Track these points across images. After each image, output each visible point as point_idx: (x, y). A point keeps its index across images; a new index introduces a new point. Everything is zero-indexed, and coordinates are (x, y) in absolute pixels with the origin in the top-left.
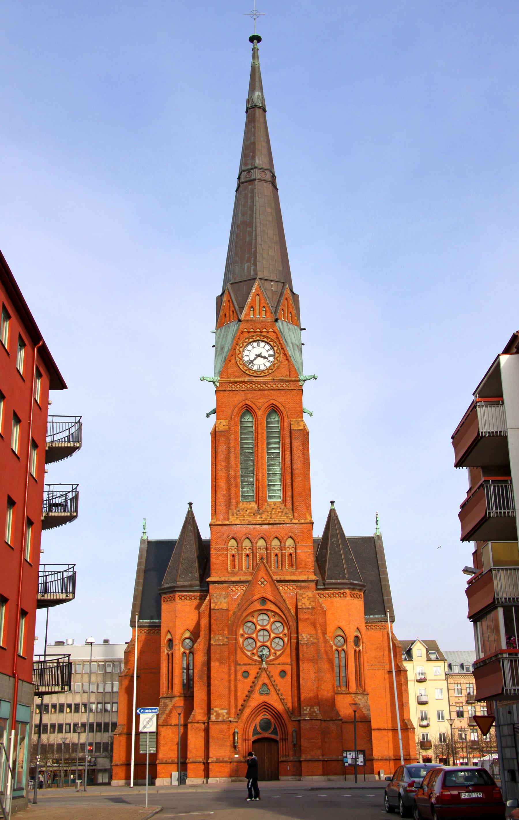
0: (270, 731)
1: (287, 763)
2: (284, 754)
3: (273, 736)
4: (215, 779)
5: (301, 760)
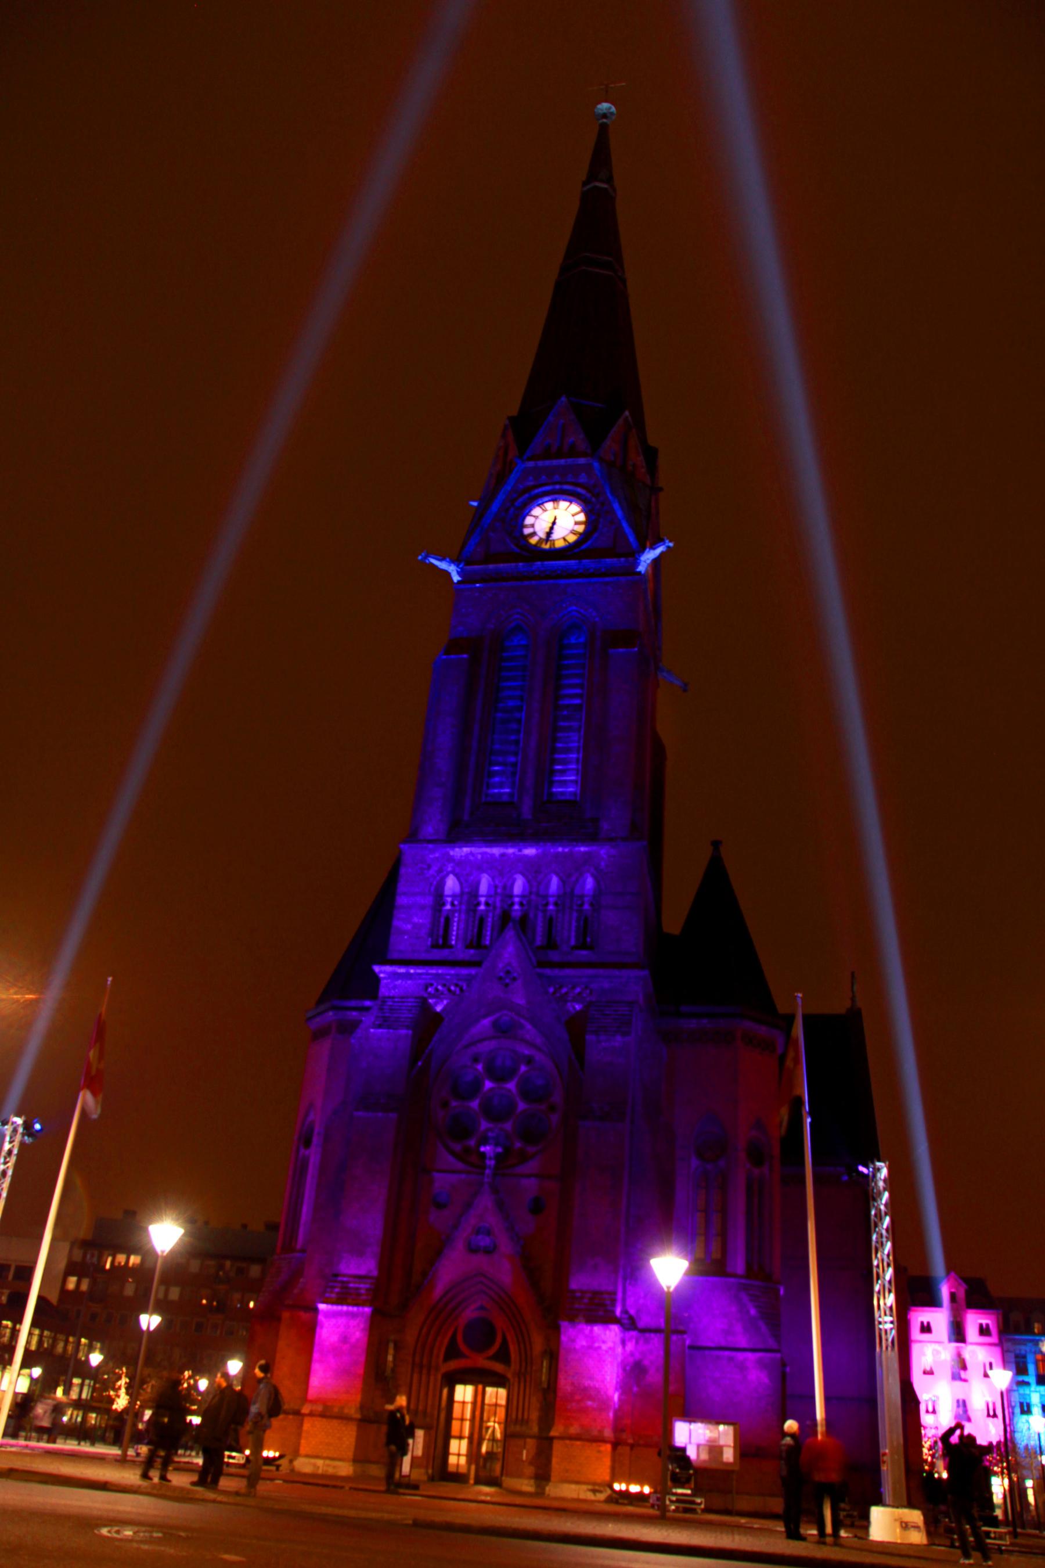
0: (493, 1351)
2: (520, 1416)
3: (498, 1367)
4: (313, 1461)
5: (553, 1433)
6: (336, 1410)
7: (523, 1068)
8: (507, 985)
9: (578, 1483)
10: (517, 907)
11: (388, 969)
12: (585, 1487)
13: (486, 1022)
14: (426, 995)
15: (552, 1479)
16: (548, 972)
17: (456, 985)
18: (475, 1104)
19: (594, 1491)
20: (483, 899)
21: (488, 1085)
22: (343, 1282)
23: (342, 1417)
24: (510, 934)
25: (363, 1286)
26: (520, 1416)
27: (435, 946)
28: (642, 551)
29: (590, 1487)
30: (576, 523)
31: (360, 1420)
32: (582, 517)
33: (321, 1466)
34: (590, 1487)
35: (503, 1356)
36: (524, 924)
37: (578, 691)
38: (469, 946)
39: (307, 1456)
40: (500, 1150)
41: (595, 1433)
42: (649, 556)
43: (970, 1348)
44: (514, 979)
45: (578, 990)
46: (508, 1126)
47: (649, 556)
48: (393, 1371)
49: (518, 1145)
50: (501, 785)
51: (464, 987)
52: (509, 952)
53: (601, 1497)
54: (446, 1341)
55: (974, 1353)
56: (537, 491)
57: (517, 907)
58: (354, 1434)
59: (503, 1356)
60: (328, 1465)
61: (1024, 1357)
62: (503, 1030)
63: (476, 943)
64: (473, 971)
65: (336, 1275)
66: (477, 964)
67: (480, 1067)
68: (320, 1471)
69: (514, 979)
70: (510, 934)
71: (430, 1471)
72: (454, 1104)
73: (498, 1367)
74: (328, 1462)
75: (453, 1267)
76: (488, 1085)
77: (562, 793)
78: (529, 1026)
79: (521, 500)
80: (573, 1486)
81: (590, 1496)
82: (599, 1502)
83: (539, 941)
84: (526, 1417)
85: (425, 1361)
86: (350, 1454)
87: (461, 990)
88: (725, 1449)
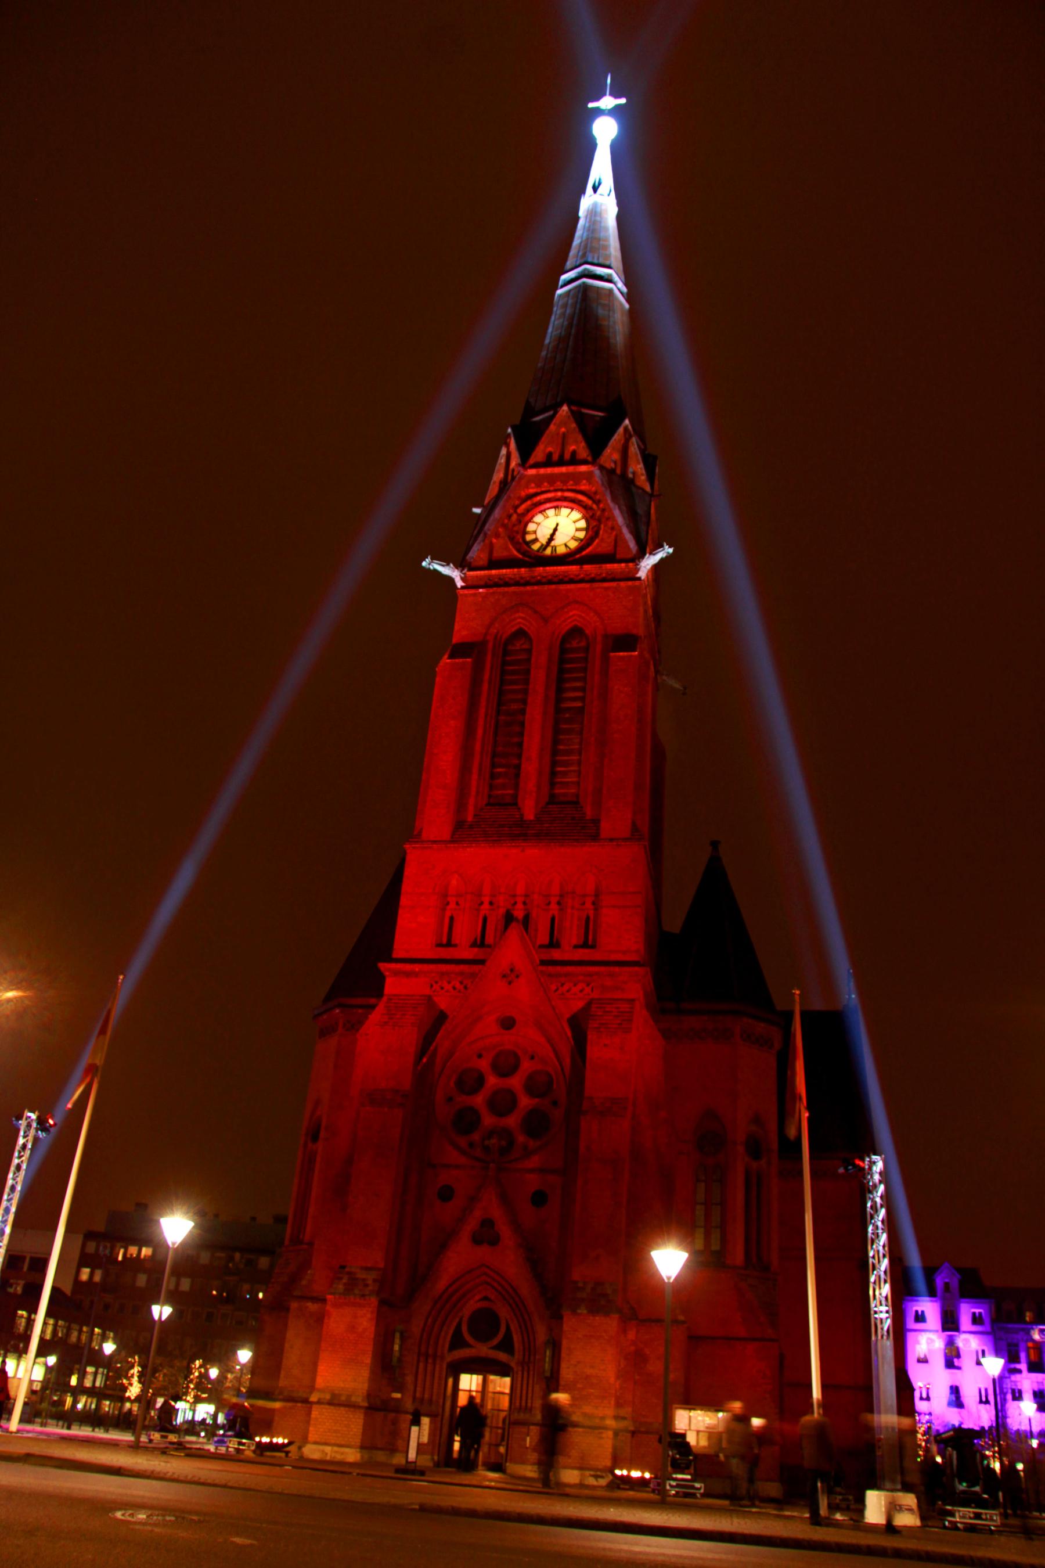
0: (495, 1341)
1: (524, 1430)
2: (523, 1404)
3: (502, 1356)
4: (321, 1447)
6: (343, 1398)
8: (510, 983)
19: (596, 1477)
25: (370, 1277)
26: (523, 1404)
28: (641, 555)
29: (592, 1473)
30: (577, 530)
31: (367, 1408)
32: (583, 524)
33: (330, 1452)
34: (592, 1473)
35: (506, 1345)
37: (580, 694)
39: (316, 1443)
43: (964, 1336)
48: (400, 1360)
53: (603, 1482)
54: (451, 1331)
55: (967, 1341)
56: (538, 498)
58: (361, 1421)
59: (506, 1345)
60: (336, 1452)
61: (1017, 1345)
62: (508, 1024)
64: (476, 968)
66: (482, 962)
68: (328, 1458)
70: (515, 931)
71: (436, 1458)
73: (502, 1356)
74: (336, 1449)
75: (459, 1257)
82: (601, 1487)
84: (529, 1405)
85: (430, 1352)
86: (358, 1441)
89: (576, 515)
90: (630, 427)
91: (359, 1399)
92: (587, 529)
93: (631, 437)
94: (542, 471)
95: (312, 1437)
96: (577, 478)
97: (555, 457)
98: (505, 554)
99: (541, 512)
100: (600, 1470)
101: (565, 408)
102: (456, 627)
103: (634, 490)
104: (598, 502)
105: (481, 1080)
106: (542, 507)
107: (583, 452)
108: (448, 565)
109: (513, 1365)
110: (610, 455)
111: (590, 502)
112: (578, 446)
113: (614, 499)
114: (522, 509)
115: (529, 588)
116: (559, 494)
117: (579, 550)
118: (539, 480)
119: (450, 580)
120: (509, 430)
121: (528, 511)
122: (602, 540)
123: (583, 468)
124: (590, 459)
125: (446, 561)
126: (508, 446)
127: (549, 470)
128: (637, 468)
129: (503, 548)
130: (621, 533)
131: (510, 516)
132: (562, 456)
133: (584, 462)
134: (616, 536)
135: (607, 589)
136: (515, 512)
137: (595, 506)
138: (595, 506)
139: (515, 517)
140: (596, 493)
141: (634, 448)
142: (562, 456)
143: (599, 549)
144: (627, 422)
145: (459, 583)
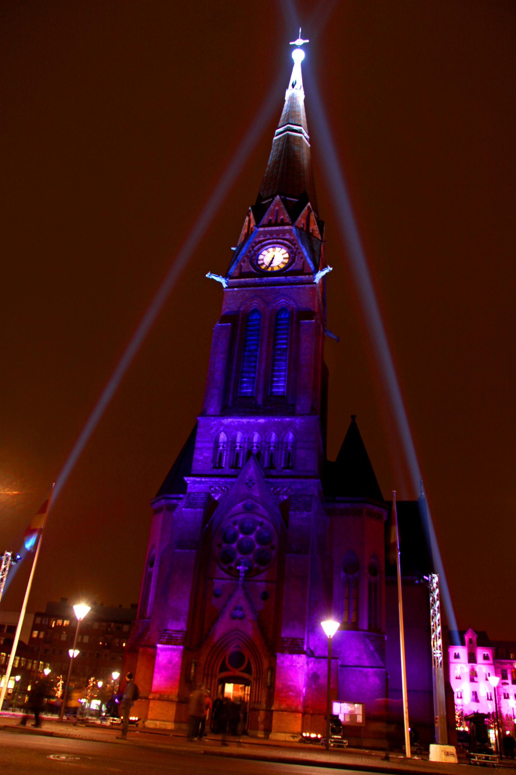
3: (246, 675)
4: (155, 722)
7: (258, 528)
8: (250, 487)
9: (285, 733)
10: (255, 448)
11: (191, 479)
12: (289, 735)
13: (240, 505)
14: (210, 492)
15: (273, 731)
16: (270, 480)
17: (225, 487)
18: (234, 546)
19: (293, 737)
20: (238, 444)
21: (241, 536)
22: (169, 634)
23: (171, 701)
24: (252, 462)
27: (214, 467)
28: (316, 271)
29: (291, 735)
30: (284, 258)
32: (287, 255)
33: (158, 724)
34: (291, 735)
35: (248, 670)
36: (258, 456)
38: (231, 467)
39: (152, 720)
40: (247, 568)
41: (294, 708)
42: (320, 275)
44: (254, 484)
45: (285, 489)
46: (251, 556)
47: (320, 275)
49: (256, 566)
50: (247, 388)
51: (229, 488)
52: (251, 471)
53: (297, 739)
57: (255, 448)
59: (248, 670)
60: (162, 724)
62: (248, 509)
63: (235, 466)
65: (166, 630)
66: (235, 476)
67: (237, 527)
68: (158, 727)
69: (254, 484)
70: (252, 462)
72: (224, 545)
73: (246, 675)
74: (162, 722)
75: (223, 627)
76: (241, 536)
77: (278, 392)
78: (261, 507)
79: (257, 247)
80: (283, 734)
81: (291, 739)
82: (296, 742)
83: (266, 465)
84: (259, 700)
85: (210, 673)
86: (173, 718)
87: (228, 489)
88: (358, 716)
89: (284, 251)
90: (311, 207)
91: (174, 697)
92: (289, 258)
93: (311, 211)
94: (266, 229)
95: (149, 717)
96: (284, 232)
97: (273, 222)
98: (248, 270)
99: (266, 250)
100: (294, 733)
101: (278, 197)
102: (223, 307)
103: (313, 238)
104: (294, 245)
105: (235, 536)
106: (266, 247)
107: (288, 220)
108: (219, 276)
109: (251, 680)
110: (301, 220)
111: (290, 245)
112: (285, 216)
113: (303, 243)
114: (255, 249)
115: (259, 288)
116: (275, 240)
117: (285, 268)
118: (265, 233)
119: (220, 284)
120: (250, 208)
121: (259, 249)
122: (297, 264)
123: (287, 227)
124: (290, 223)
125: (218, 274)
126: (249, 216)
127: (270, 229)
128: (314, 227)
129: (247, 267)
130: (306, 260)
131: (250, 252)
132: (276, 220)
133: (288, 224)
134: (304, 262)
135: (299, 288)
136: (253, 250)
137: (293, 247)
138: (293, 247)
139: (252, 252)
140: (293, 240)
141: (313, 217)
142: (276, 220)
143: (295, 268)
144: (309, 204)
145: (225, 286)
